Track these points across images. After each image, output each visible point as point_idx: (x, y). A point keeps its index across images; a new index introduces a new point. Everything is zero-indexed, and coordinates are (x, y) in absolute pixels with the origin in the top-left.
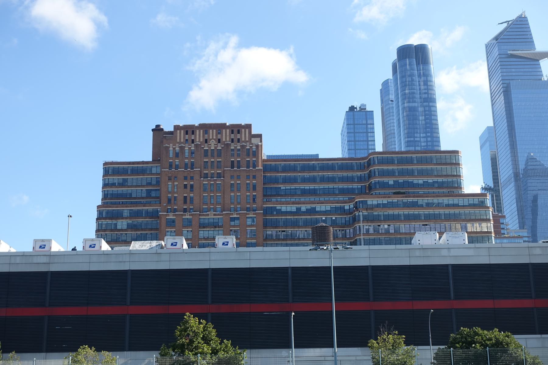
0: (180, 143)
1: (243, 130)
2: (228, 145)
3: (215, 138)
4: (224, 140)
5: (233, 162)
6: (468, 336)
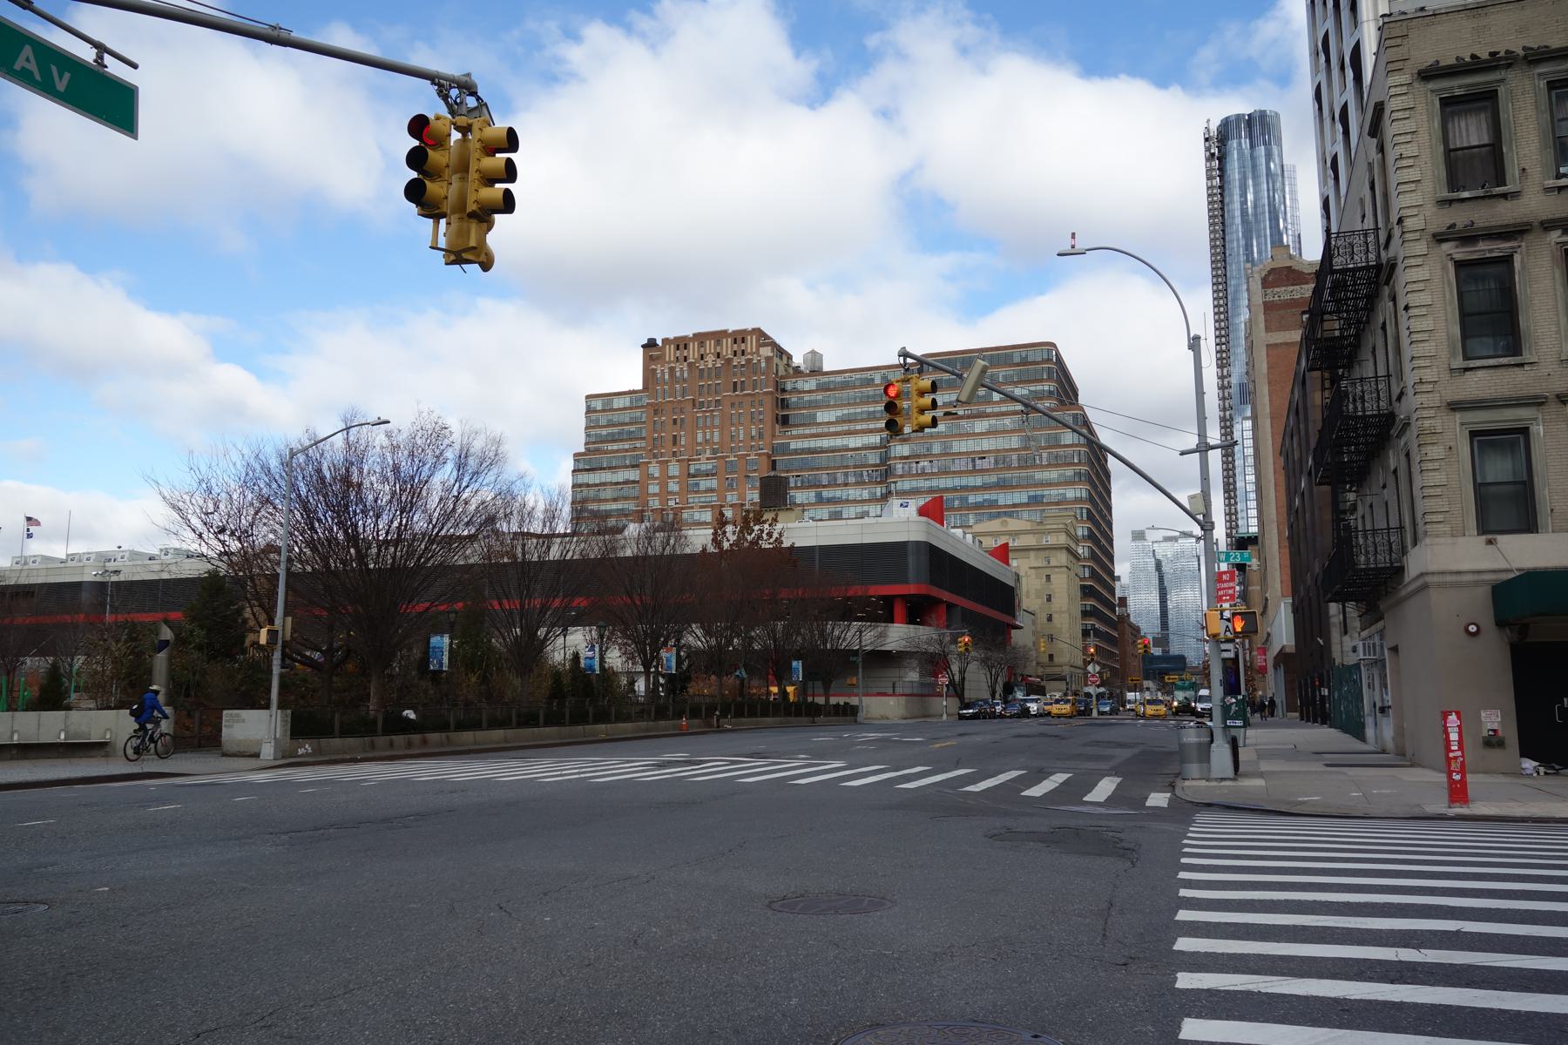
0: (670, 362)
1: (749, 338)
2: (729, 361)
3: (713, 351)
4: (724, 353)
5: (735, 383)
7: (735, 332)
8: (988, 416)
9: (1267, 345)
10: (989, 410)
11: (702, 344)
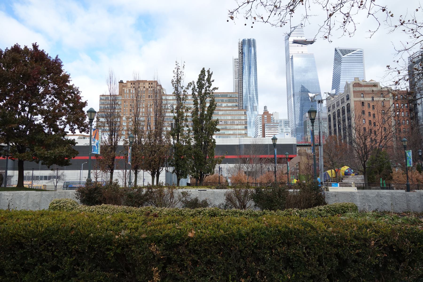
0: (129, 88)
2: (147, 89)
7: (149, 81)
8: (222, 110)
9: (354, 101)
10: (221, 109)
11: (139, 84)
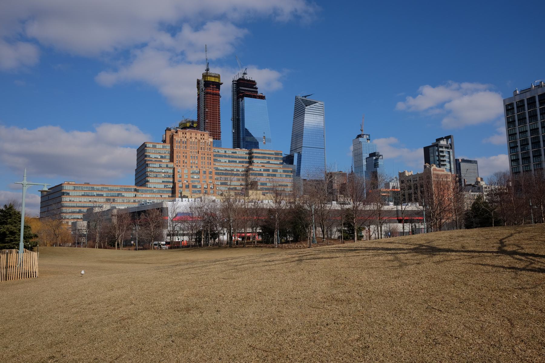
0: (180, 137)
2: (199, 140)
6: (257, 214)
